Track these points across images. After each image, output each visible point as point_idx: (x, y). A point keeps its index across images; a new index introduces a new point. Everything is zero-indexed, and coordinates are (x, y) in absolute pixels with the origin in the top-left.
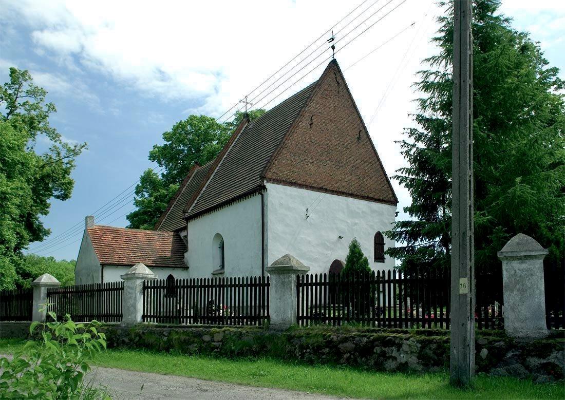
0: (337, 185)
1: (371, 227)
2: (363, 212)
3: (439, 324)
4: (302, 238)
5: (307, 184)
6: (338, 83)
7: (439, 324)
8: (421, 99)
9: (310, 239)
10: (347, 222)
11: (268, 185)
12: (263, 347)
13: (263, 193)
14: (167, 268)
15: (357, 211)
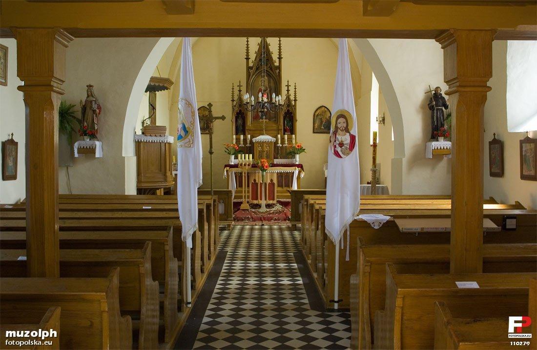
3: (11, 336)
7: (11, 336)
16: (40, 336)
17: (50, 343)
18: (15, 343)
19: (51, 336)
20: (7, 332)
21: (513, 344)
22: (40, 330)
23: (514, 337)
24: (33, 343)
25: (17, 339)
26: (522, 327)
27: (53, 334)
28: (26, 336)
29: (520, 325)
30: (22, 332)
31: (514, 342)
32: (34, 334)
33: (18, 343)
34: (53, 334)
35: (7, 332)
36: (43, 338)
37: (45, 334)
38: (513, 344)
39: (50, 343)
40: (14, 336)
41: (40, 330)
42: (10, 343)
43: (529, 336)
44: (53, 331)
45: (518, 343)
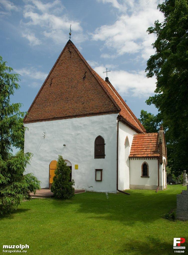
0: (66, 112)
1: (92, 134)
2: (84, 125)
3: (5, 248)
4: (41, 149)
6: (71, 52)
7: (5, 248)
8: (146, 69)
9: (46, 149)
10: (72, 135)
11: (25, 125)
12: (21, 210)
15: (79, 125)
16: (20, 248)
17: (26, 251)
18: (7, 251)
19: (26, 248)
20: (4, 246)
21: (176, 252)
22: (20, 245)
23: (176, 248)
24: (17, 251)
25: (8, 249)
26: (180, 243)
27: (27, 247)
28: (13, 248)
29: (179, 242)
30: (11, 246)
31: (176, 251)
32: (18, 247)
33: (9, 251)
34: (27, 247)
35: (4, 246)
36: (22, 249)
37: (23, 247)
38: (176, 252)
39: (26, 251)
40: (7, 248)
41: (20, 245)
42: (5, 251)
43: (184, 248)
44: (27, 245)
45: (178, 252)
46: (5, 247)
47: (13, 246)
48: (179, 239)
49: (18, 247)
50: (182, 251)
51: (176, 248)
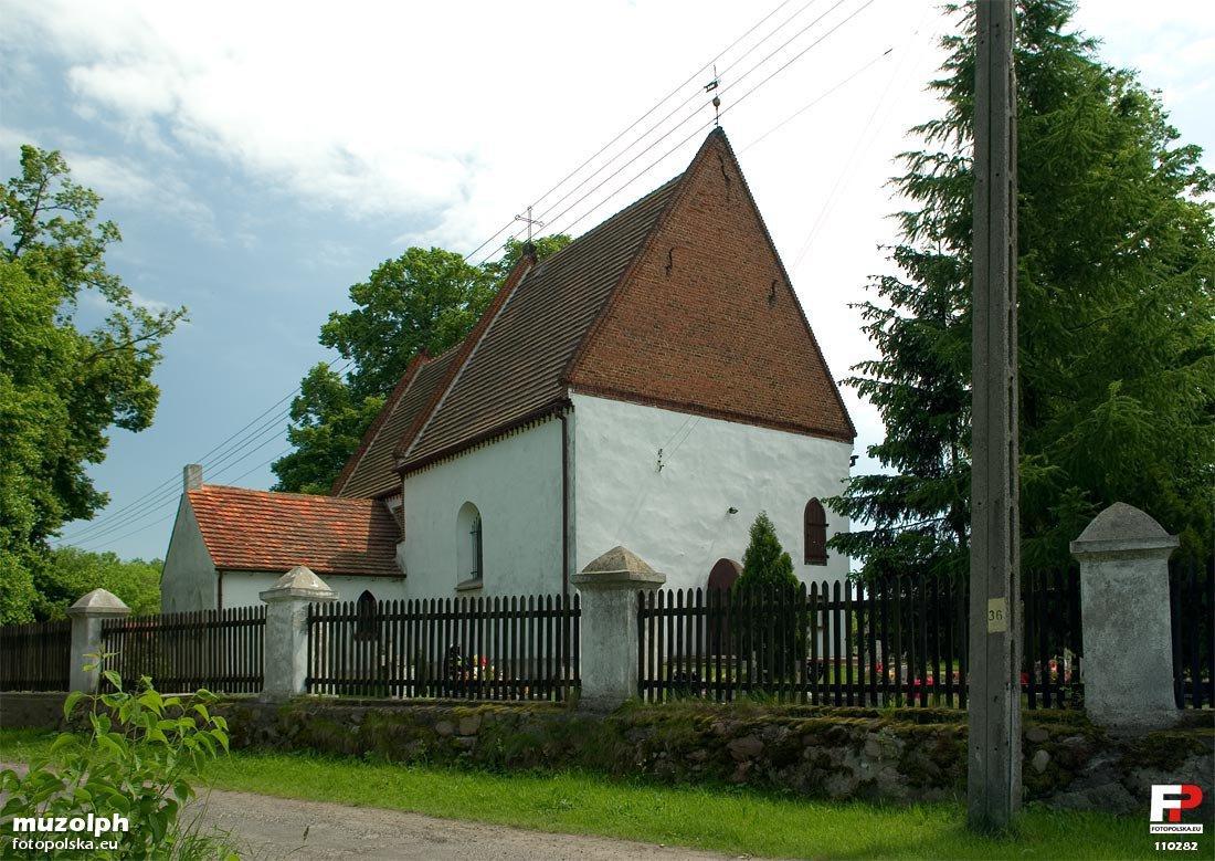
2: (781, 457)
4: (649, 512)
5: (661, 396)
7: (24, 829)
9: (667, 515)
10: (746, 479)
13: (565, 415)
14: (359, 578)
15: (768, 453)
16: (90, 829)
17: (113, 845)
18: (33, 845)
19: (115, 829)
21: (1161, 846)
24: (75, 844)
25: (37, 836)
27: (120, 824)
29: (1176, 804)
30: (50, 821)
31: (1164, 844)
32: (77, 825)
34: (120, 824)
36: (97, 834)
37: (103, 824)
38: (1161, 846)
39: (113, 845)
42: (23, 845)
45: (1171, 846)
46: (20, 825)
47: (57, 819)
48: (1177, 789)
49: (81, 828)
50: (1187, 844)
51: (1160, 832)
